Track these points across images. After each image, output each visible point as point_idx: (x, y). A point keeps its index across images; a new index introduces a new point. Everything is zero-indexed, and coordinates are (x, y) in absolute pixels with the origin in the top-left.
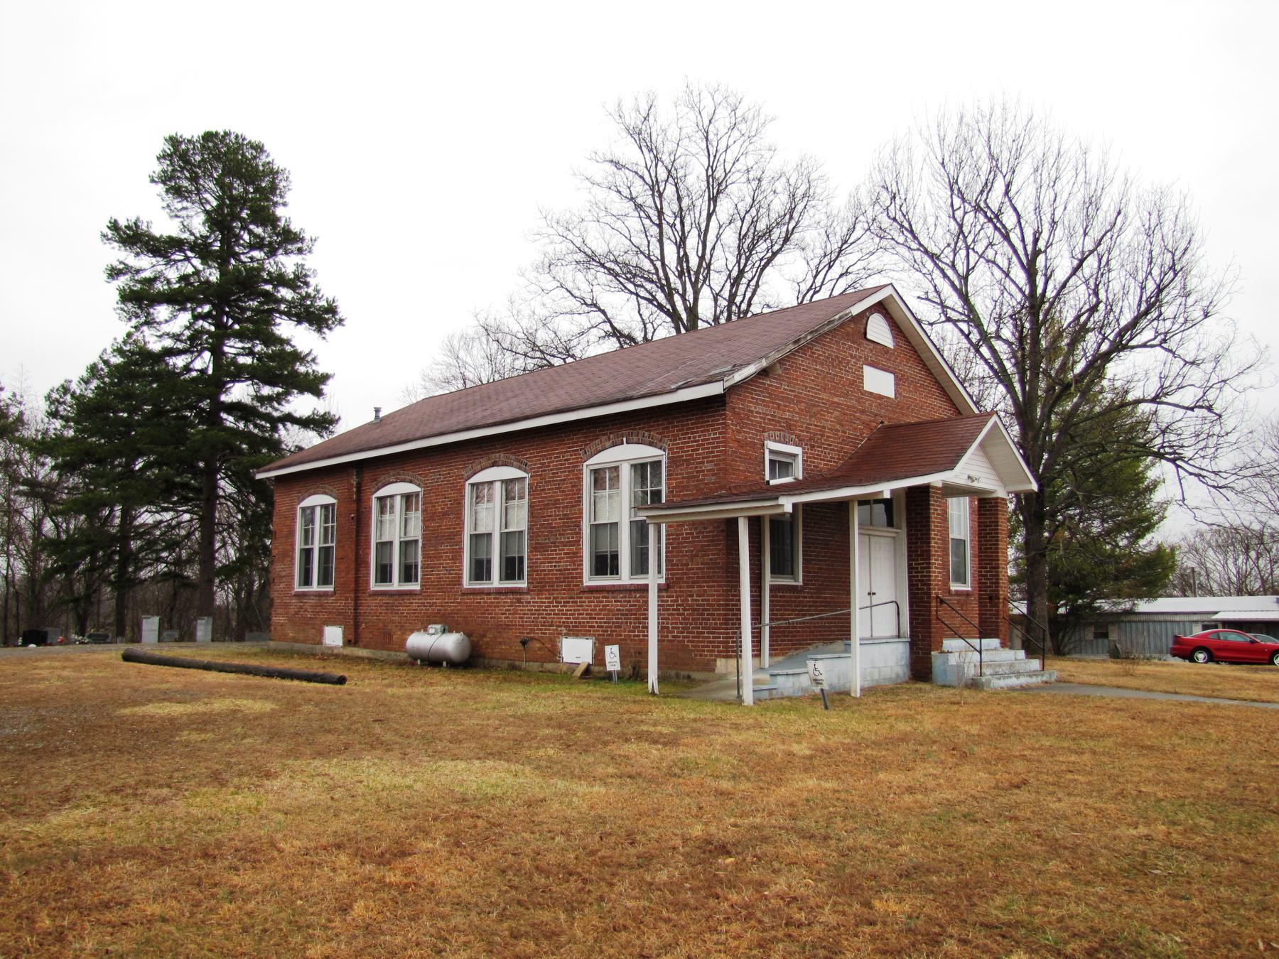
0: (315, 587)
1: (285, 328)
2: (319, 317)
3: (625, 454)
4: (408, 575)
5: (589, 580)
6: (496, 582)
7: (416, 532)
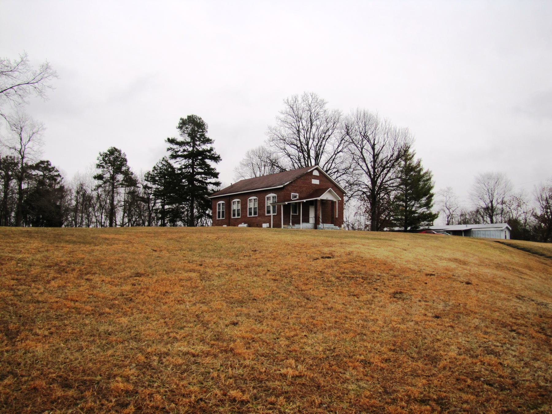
0: (221, 218)
1: (208, 161)
2: (216, 159)
3: (271, 195)
4: (238, 215)
5: (266, 215)
6: (253, 215)
7: (240, 208)
